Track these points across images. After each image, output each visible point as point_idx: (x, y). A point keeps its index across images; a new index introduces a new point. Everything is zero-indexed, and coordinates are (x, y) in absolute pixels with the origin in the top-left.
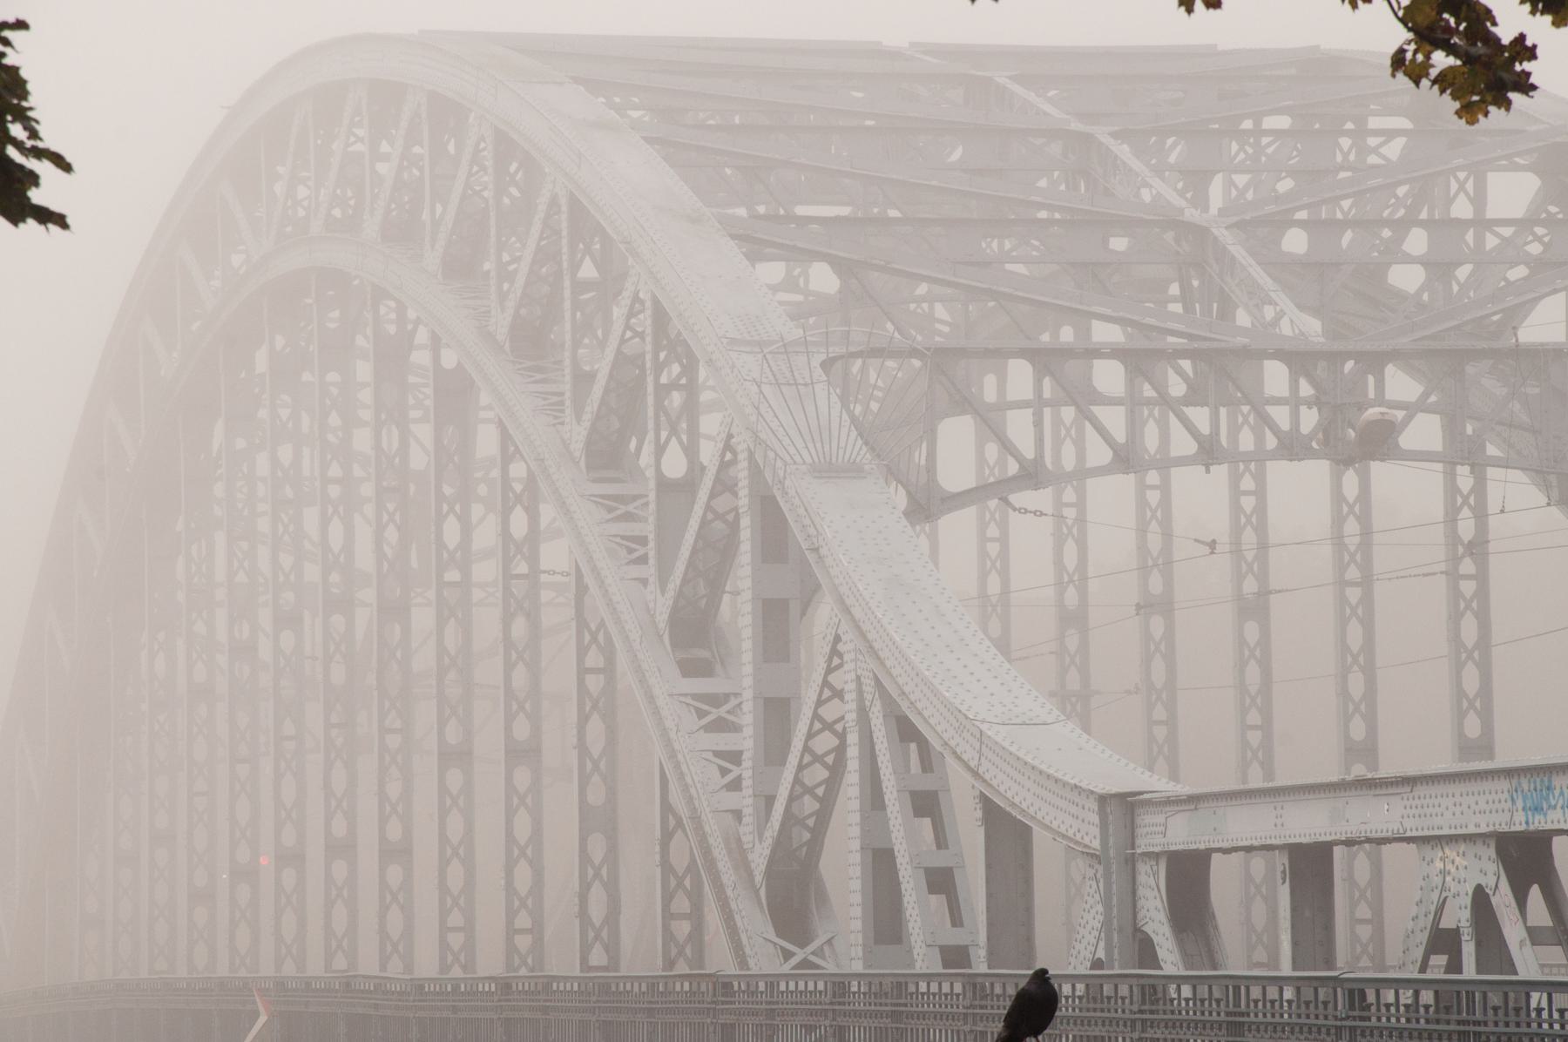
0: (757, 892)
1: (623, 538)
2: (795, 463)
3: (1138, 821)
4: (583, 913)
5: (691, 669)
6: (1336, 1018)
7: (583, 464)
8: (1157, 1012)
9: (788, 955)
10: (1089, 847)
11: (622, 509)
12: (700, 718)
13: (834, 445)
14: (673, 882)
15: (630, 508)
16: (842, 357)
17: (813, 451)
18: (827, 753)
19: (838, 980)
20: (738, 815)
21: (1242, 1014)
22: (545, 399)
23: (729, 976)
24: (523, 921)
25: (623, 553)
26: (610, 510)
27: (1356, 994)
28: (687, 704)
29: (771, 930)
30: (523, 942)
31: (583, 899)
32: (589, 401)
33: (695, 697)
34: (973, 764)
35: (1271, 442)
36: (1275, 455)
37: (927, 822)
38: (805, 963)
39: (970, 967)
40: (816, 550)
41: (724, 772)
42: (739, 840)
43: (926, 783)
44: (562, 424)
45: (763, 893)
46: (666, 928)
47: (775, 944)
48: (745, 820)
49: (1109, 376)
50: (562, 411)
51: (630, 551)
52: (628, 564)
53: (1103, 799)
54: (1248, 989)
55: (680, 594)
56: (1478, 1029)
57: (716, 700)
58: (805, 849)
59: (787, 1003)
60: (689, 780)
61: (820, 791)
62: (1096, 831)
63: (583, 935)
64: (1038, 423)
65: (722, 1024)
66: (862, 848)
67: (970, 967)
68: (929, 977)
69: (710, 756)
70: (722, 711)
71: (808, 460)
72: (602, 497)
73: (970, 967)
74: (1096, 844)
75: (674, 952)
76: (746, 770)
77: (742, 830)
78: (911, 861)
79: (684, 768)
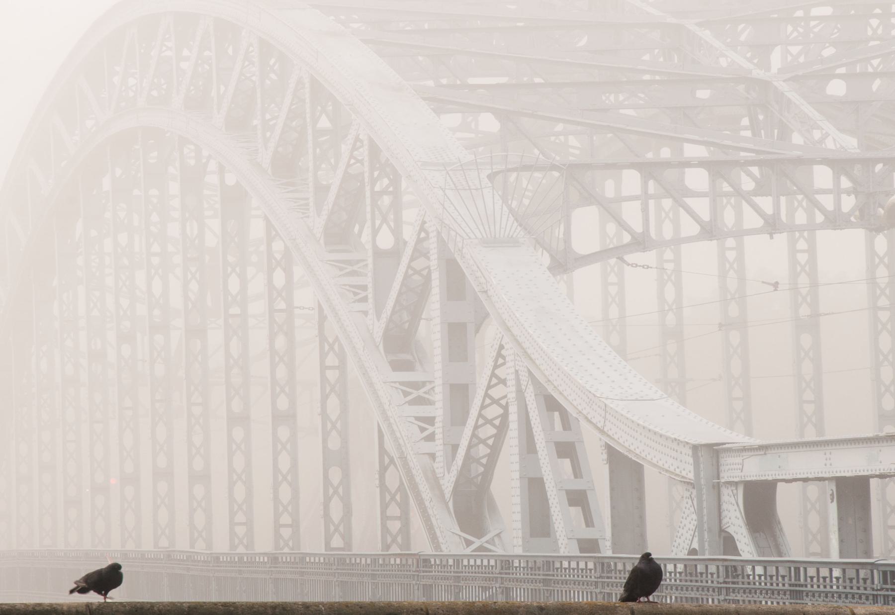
0: (447, 504)
2: (470, 238)
3: (722, 461)
4: (327, 515)
5: (397, 366)
6: (873, 589)
9: (469, 543)
10: (686, 478)
11: (350, 269)
14: (388, 498)
20: (433, 456)
21: (802, 586)
24: (286, 519)
26: (341, 269)
28: (396, 388)
30: (286, 533)
33: (402, 383)
34: (599, 425)
35: (820, 218)
36: (822, 227)
38: (481, 548)
39: (599, 552)
41: (423, 430)
42: (434, 471)
45: (451, 505)
47: (459, 535)
48: (437, 460)
49: (697, 179)
51: (355, 294)
52: (354, 302)
53: (695, 448)
57: (416, 386)
58: (480, 478)
61: (490, 442)
62: (692, 468)
64: (645, 210)
65: (423, 585)
67: (599, 552)
68: (570, 558)
69: (413, 420)
70: (421, 392)
74: (691, 476)
76: (438, 428)
77: (436, 465)
79: (395, 427)
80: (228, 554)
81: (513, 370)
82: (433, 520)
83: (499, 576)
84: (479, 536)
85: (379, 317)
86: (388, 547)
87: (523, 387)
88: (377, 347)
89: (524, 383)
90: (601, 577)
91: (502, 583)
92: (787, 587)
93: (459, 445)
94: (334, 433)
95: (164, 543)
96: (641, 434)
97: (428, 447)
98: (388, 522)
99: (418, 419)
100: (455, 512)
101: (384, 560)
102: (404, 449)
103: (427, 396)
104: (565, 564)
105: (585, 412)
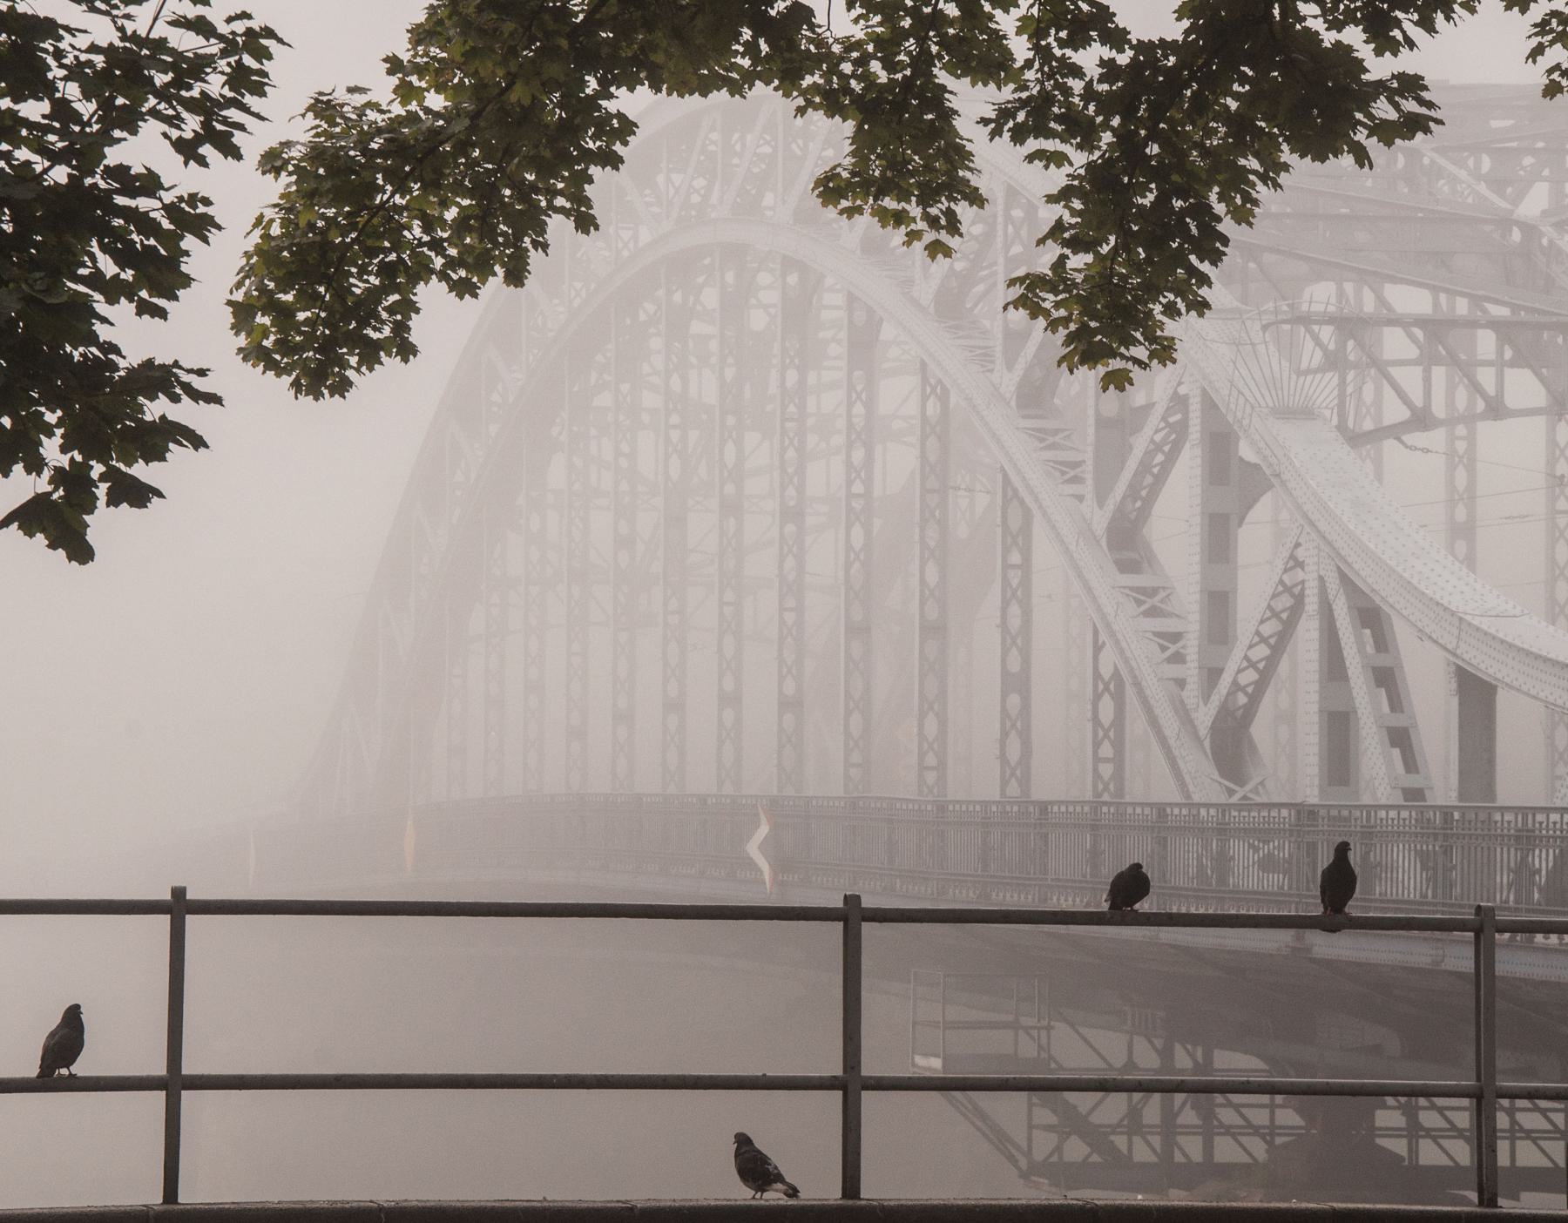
1: (1055, 462)
2: (1260, 406)
4: (1003, 757)
5: (1126, 567)
7: (1013, 403)
8: (1317, 826)
9: (1231, 792)
11: (1051, 440)
12: (1138, 606)
13: (1286, 393)
14: (1101, 734)
15: (1057, 439)
16: (1273, 323)
17: (1275, 398)
18: (1271, 636)
19: (1311, 808)
20: (1181, 683)
22: (971, 351)
23: (1314, 805)
24: (931, 760)
25: (1057, 474)
26: (1042, 440)
27: (1044, 807)
28: (1127, 595)
29: (1217, 773)
30: (931, 777)
31: (1003, 743)
32: (1022, 354)
33: (1132, 589)
34: (1449, 647)
35: (1481, 405)
36: (1484, 416)
37: (1383, 691)
38: (1245, 798)
40: (1278, 475)
42: (1182, 702)
43: (1383, 661)
44: (991, 371)
45: (1207, 744)
46: (1095, 770)
47: (1220, 783)
50: (993, 362)
51: (1063, 473)
54: (1376, 812)
55: (1120, 509)
56: (1529, 834)
59: (1463, 829)
60: (1128, 654)
63: (1003, 773)
66: (1320, 711)
67: (1425, 801)
68: (1388, 807)
69: (1148, 635)
70: (1156, 600)
71: (1271, 405)
72: (1033, 429)
73: (1425, 801)
75: (1101, 787)
77: (1185, 694)
78: (1376, 722)
79: (1124, 645)
80: (999, 802)
81: (1315, 575)
82: (1181, 763)
83: (1441, 831)
84: (1241, 782)
85: (1101, 505)
86: (1100, 796)
87: (1330, 597)
88: (1098, 541)
89: (1332, 593)
90: (1040, 819)
91: (1159, 832)
92: (1358, 829)
93: (1223, 669)
94: (1014, 651)
95: (728, 789)
96: (1514, 659)
97: (1174, 671)
98: (1100, 764)
99: (1158, 634)
100: (1213, 753)
101: (1463, 815)
102: (1137, 672)
103: (1163, 606)
104: (1056, 808)
105: (1427, 630)
